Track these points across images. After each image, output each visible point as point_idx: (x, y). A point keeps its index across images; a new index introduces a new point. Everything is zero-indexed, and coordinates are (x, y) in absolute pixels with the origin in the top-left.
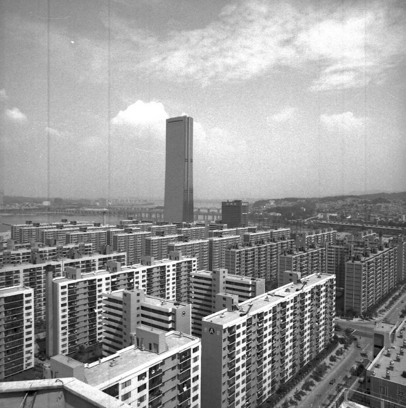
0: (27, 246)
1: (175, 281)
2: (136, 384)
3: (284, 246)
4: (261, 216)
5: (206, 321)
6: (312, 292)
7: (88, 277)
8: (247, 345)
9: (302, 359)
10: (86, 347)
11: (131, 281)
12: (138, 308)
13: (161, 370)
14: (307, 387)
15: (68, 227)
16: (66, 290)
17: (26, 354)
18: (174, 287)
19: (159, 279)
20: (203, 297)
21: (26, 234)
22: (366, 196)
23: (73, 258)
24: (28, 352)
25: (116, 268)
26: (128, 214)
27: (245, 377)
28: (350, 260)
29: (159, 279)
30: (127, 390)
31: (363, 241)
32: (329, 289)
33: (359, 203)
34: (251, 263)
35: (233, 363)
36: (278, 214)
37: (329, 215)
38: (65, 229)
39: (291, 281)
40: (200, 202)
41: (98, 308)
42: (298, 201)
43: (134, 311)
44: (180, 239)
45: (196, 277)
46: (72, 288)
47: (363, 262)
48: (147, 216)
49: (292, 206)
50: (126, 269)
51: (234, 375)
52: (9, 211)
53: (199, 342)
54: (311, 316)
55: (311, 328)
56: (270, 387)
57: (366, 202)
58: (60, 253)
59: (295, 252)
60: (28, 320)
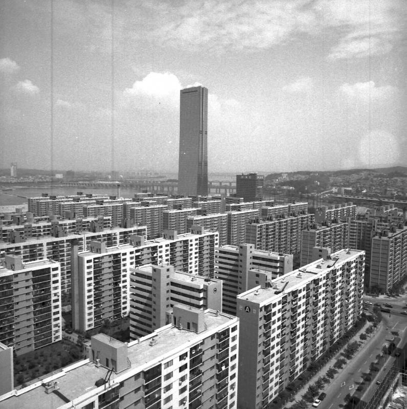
0: (46, 219)
1: (197, 255)
2: (178, 364)
3: (304, 221)
4: (274, 190)
5: (242, 298)
6: (343, 269)
7: (112, 251)
8: (282, 324)
9: (332, 337)
10: (111, 321)
11: (155, 255)
12: (168, 284)
13: (201, 350)
14: (339, 364)
15: (84, 200)
16: (92, 264)
17: (54, 327)
18: (196, 262)
19: (182, 253)
20: (228, 272)
23: (94, 231)
24: (56, 325)
25: (140, 242)
27: (279, 355)
29: (182, 253)
30: (169, 370)
31: (385, 216)
32: (359, 265)
33: (375, 177)
34: (272, 238)
37: (343, 189)
38: (83, 202)
39: (320, 256)
40: (218, 175)
41: (123, 283)
43: (164, 288)
44: (199, 213)
45: (221, 252)
46: (97, 262)
47: (390, 238)
48: (159, 189)
50: (148, 244)
53: (238, 321)
54: (342, 294)
55: (341, 306)
56: (302, 365)
57: (381, 176)
59: (318, 227)
60: (55, 295)
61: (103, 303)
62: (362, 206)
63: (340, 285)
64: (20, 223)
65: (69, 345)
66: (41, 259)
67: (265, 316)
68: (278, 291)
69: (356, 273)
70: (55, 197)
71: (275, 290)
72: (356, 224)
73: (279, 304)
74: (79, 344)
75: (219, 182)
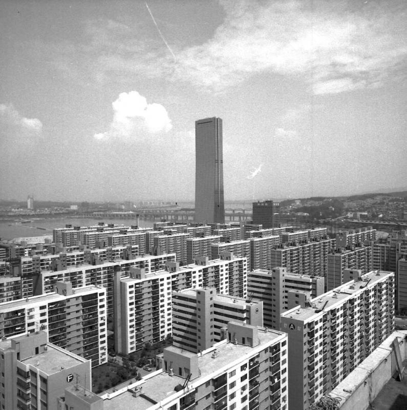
1: (228, 280)
4: (288, 216)
5: (285, 317)
6: (374, 289)
12: (211, 306)
13: (257, 362)
16: (133, 289)
18: (227, 287)
19: (214, 278)
21: (68, 237)
22: (397, 194)
23: (127, 259)
24: (103, 348)
25: (175, 268)
26: (155, 216)
28: (402, 258)
29: (214, 278)
32: (389, 287)
33: (390, 201)
34: (296, 263)
35: (312, 358)
36: (305, 214)
37: (359, 214)
40: (230, 203)
42: (325, 200)
43: (208, 309)
44: (222, 240)
46: (138, 287)
49: (318, 205)
51: (314, 369)
52: (38, 216)
53: (286, 336)
54: (375, 314)
55: (375, 326)
57: (397, 200)
58: (38, 264)
59: (343, 251)
60: (102, 319)
61: (143, 327)
62: (381, 231)
63: (372, 305)
64: (55, 252)
65: (115, 367)
66: (80, 286)
67: (308, 333)
68: (318, 310)
69: (386, 294)
70: (79, 228)
71: (315, 309)
72: (379, 248)
73: (321, 322)
74: (125, 366)
75: (242, 210)
